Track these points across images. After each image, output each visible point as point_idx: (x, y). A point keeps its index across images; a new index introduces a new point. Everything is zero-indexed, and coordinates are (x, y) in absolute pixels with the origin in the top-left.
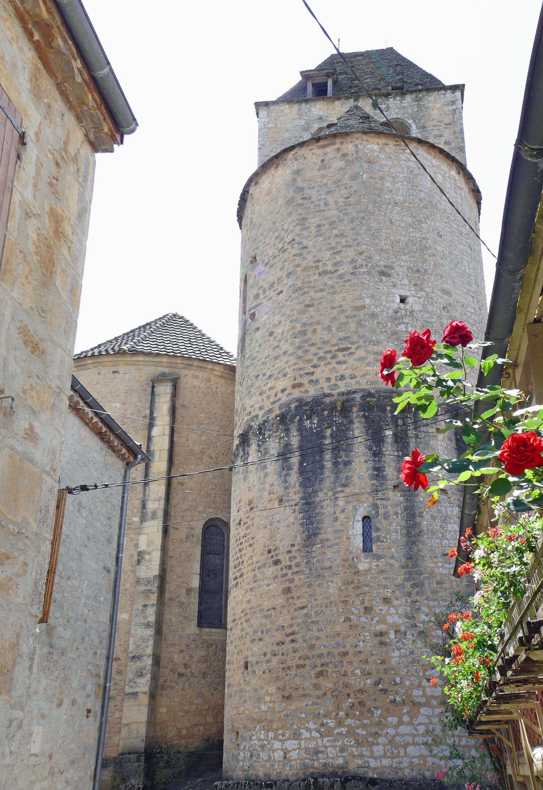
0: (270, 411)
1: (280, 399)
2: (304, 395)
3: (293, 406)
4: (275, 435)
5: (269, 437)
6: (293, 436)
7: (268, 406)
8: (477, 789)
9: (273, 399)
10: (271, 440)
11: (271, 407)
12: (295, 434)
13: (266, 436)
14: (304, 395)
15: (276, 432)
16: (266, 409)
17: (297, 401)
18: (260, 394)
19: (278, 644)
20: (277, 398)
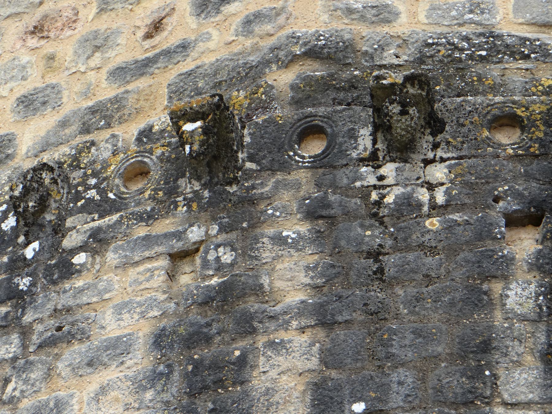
0: (104, 114)
1: (184, 47)
2: (364, 30)
3: (282, 79)
4: (141, 231)
5: (97, 242)
6: (280, 240)
7: (85, 84)
8: (284, 370)
9: (128, 48)
10: (112, 257)
11: (107, 91)
12: (295, 228)
13: (70, 241)
14: (364, 30)
15: (148, 218)
16: (72, 103)
17: (313, 53)
18: (37, 30)
19: (148, 36)
20: (167, 39)
